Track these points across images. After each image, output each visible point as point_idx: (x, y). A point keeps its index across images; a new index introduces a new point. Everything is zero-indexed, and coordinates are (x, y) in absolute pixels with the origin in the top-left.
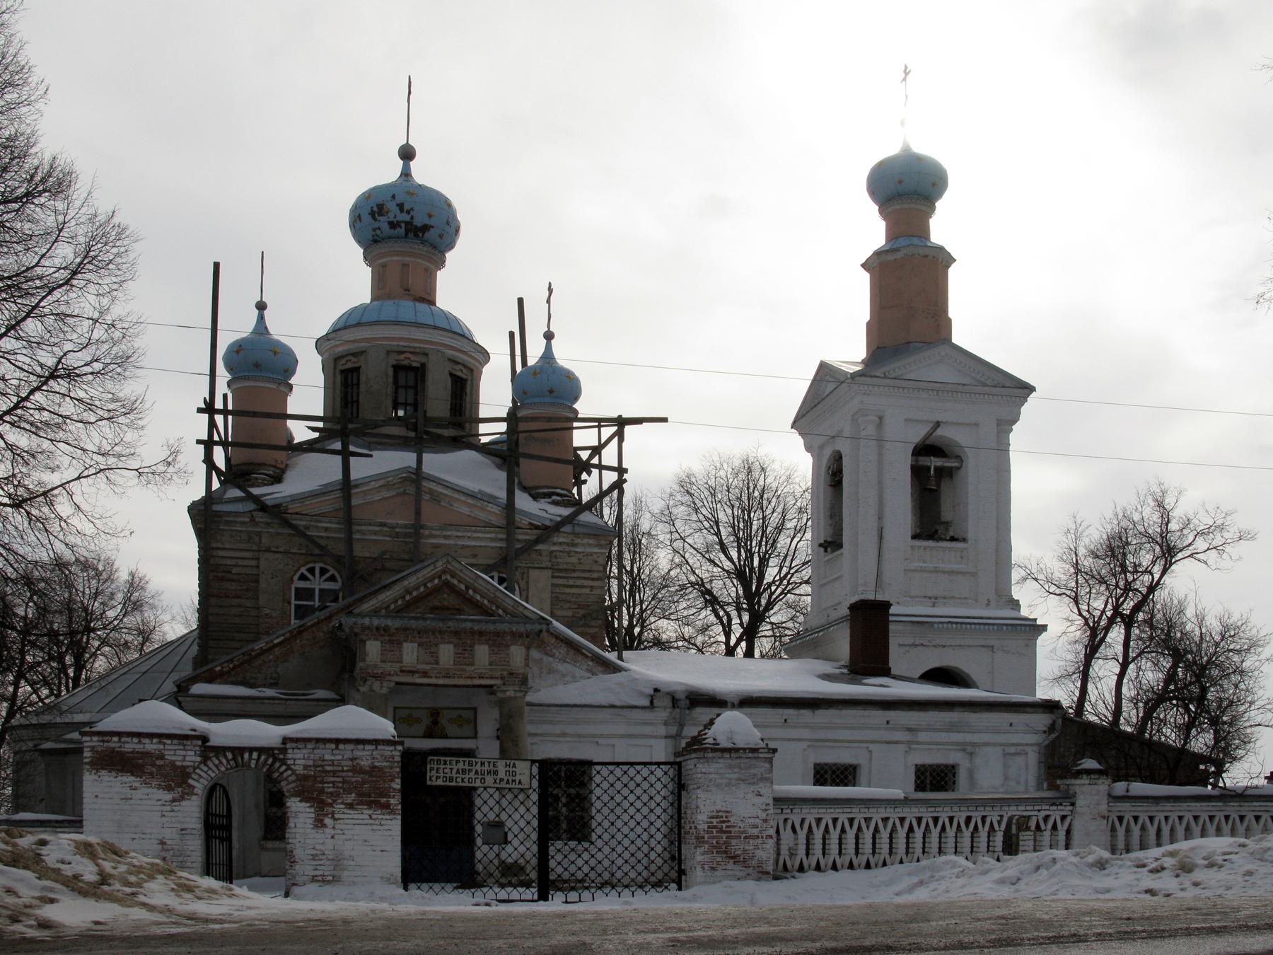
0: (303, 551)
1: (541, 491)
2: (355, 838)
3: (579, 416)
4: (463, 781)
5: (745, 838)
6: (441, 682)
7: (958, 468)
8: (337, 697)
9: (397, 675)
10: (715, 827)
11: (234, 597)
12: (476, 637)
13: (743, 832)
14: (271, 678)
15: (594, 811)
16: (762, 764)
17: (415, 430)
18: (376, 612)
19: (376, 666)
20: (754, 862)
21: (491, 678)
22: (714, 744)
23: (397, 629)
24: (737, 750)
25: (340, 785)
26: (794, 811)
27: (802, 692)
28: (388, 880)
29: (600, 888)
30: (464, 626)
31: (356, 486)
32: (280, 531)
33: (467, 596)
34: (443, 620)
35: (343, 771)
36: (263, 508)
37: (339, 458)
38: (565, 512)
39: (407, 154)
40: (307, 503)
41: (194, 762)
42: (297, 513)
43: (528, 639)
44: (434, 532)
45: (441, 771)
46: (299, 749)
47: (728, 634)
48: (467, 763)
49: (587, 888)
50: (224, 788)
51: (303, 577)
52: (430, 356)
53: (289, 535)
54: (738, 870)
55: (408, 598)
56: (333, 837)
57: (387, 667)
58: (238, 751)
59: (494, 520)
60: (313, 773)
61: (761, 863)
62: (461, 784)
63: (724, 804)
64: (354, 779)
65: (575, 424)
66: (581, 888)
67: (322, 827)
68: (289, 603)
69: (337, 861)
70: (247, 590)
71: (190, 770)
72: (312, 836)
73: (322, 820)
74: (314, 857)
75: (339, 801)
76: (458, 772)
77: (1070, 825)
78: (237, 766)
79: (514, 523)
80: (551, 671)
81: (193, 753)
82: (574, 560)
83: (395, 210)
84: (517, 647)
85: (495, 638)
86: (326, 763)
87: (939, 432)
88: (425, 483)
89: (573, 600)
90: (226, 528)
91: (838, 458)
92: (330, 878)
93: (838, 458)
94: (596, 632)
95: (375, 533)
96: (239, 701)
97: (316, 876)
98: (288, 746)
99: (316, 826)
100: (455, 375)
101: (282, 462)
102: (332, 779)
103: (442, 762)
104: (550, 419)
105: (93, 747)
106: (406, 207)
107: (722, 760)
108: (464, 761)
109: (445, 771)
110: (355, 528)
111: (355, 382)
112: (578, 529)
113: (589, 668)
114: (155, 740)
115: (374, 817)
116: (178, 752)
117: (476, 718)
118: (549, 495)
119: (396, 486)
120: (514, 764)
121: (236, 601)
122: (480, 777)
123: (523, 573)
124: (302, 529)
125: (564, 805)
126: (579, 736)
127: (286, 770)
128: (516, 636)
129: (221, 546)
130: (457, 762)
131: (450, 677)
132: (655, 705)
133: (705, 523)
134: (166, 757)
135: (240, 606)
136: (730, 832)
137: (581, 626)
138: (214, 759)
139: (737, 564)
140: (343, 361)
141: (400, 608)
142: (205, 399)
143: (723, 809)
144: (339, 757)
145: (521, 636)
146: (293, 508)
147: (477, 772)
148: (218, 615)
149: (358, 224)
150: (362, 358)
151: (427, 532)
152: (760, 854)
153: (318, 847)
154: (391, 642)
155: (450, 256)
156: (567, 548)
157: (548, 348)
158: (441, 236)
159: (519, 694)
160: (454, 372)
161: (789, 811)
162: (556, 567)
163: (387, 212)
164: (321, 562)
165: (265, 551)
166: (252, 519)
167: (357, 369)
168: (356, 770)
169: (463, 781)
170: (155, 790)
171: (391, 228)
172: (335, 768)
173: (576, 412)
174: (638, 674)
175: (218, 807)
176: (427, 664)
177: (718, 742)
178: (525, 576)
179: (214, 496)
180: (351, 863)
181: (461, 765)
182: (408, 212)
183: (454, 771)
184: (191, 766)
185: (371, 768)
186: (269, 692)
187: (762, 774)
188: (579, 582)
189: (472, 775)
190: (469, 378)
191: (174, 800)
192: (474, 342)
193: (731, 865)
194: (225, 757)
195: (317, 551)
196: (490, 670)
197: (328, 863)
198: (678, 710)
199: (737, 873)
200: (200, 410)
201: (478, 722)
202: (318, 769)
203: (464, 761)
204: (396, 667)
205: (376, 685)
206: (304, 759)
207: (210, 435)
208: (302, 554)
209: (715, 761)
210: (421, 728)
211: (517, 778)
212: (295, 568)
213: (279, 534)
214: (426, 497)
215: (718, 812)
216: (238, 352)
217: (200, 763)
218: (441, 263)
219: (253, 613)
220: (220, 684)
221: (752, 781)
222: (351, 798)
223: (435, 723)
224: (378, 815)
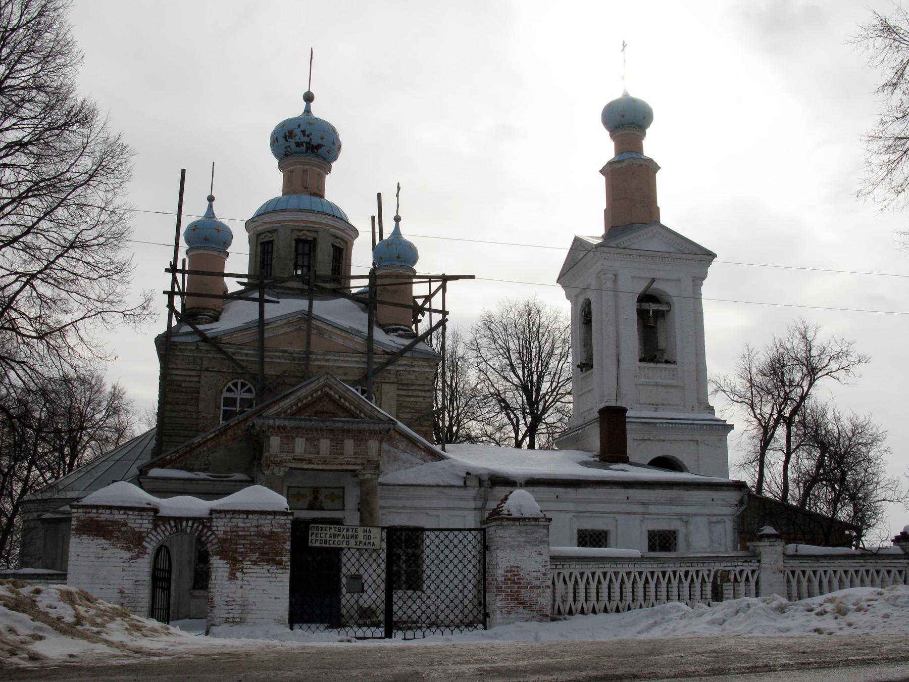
0: (231, 370)
2: (257, 588)
3: (417, 274)
4: (334, 543)
5: (531, 587)
6: (320, 467)
7: (668, 311)
8: (249, 479)
10: (509, 579)
12: (346, 434)
13: (530, 583)
15: (425, 567)
16: (542, 530)
17: (308, 284)
18: (277, 415)
19: (276, 455)
20: (537, 607)
21: (355, 464)
22: (508, 515)
23: (292, 428)
24: (524, 519)
25: (248, 546)
28: (280, 621)
29: (428, 628)
31: (268, 324)
32: (215, 356)
34: (323, 421)
35: (250, 535)
36: (205, 339)
37: (257, 304)
38: (407, 342)
39: (309, 98)
41: (148, 529)
42: (227, 343)
44: (319, 357)
47: (516, 431)
49: (419, 628)
51: (229, 390)
53: (222, 359)
54: (526, 613)
55: (300, 405)
56: (241, 587)
57: (284, 456)
58: (179, 520)
60: (229, 537)
61: (542, 608)
62: (332, 546)
64: (258, 542)
65: (414, 280)
66: (415, 628)
68: (219, 409)
69: (244, 607)
71: (144, 535)
72: (226, 586)
73: (234, 574)
76: (330, 536)
77: (758, 577)
80: (396, 459)
81: (147, 522)
82: (412, 377)
86: (239, 529)
87: (655, 285)
88: (314, 322)
91: (588, 304)
92: (238, 620)
93: (588, 304)
95: (279, 357)
96: (181, 481)
97: (228, 618)
98: (214, 516)
99: (230, 579)
104: (397, 277)
105: (78, 517)
106: (307, 133)
107: (513, 527)
110: (266, 354)
111: (270, 250)
112: (415, 355)
114: (122, 512)
115: (271, 571)
117: (344, 494)
118: (396, 330)
121: (183, 407)
122: (346, 540)
124: (230, 354)
125: (404, 562)
126: (416, 508)
127: (211, 535)
128: (373, 433)
129: (175, 367)
130: (330, 528)
131: (326, 464)
134: (129, 525)
135: (186, 411)
136: (520, 583)
138: (162, 526)
140: (263, 237)
143: (515, 565)
144: (249, 525)
145: (376, 432)
146: (225, 339)
147: (343, 536)
148: (170, 417)
150: (275, 234)
151: (314, 357)
153: (231, 595)
154: (287, 437)
156: (408, 369)
158: (329, 152)
161: (561, 567)
163: (295, 136)
166: (197, 348)
167: (271, 242)
168: (260, 535)
169: (334, 543)
172: (245, 533)
173: (415, 272)
176: (312, 454)
179: (172, 330)
180: (253, 607)
181: (333, 531)
182: (308, 136)
183: (328, 536)
186: (203, 475)
187: (541, 538)
188: (415, 393)
189: (340, 538)
191: (132, 558)
193: (521, 610)
194: (170, 525)
195: (240, 371)
196: (355, 458)
197: (238, 607)
198: (483, 489)
200: (167, 270)
205: (276, 470)
207: (173, 288)
210: (305, 503)
211: (371, 541)
213: (214, 358)
214: (314, 331)
215: (511, 567)
216: (194, 230)
217: (152, 529)
218: (328, 170)
220: (169, 468)
221: (535, 543)
223: (316, 498)
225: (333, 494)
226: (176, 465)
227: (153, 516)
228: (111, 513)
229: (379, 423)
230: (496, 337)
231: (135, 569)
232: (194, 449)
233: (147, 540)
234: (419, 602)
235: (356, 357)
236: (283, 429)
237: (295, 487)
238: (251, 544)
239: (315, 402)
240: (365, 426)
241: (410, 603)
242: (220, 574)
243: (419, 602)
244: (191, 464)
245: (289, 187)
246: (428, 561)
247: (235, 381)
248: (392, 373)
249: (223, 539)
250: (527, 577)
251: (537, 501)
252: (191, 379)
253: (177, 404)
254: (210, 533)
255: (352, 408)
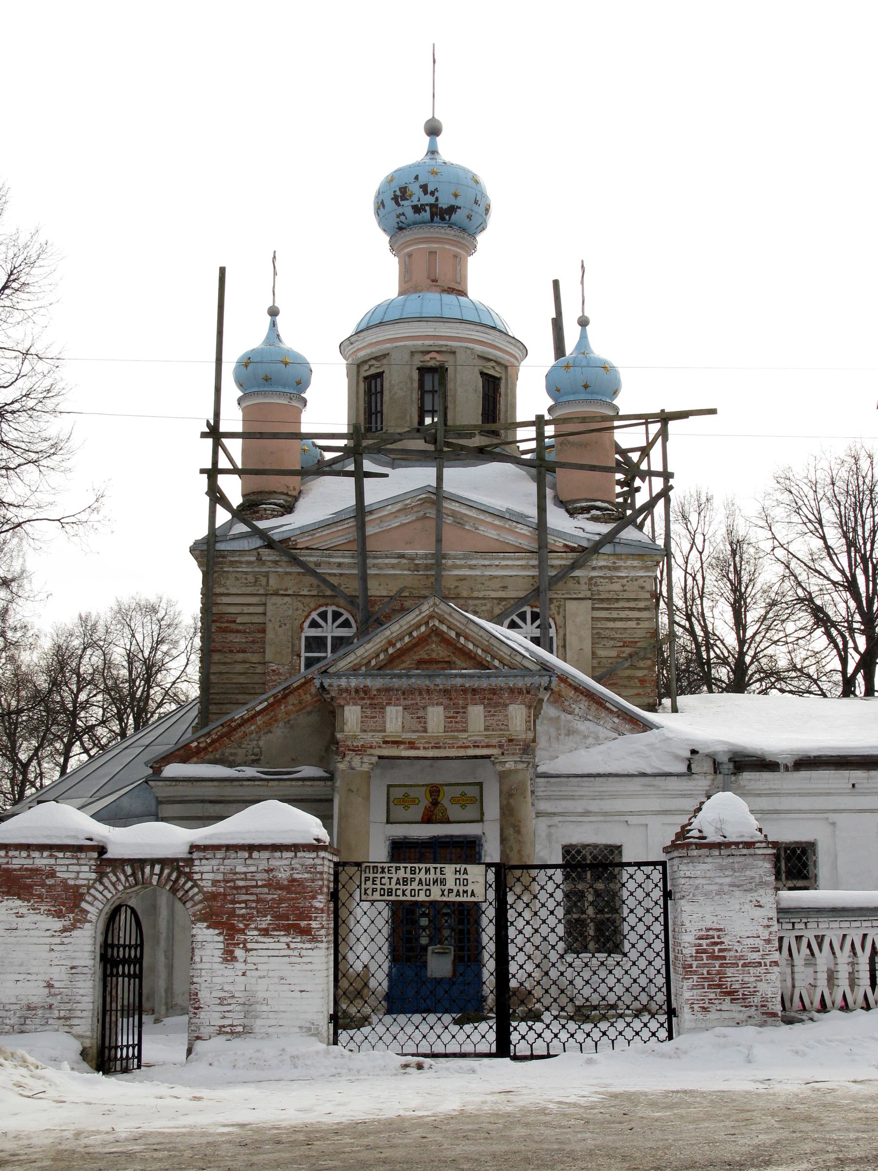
0: (314, 593)
1: (578, 505)
2: (271, 974)
3: (620, 414)
4: (404, 894)
5: (744, 965)
6: (430, 753)
8: (326, 775)
9: (380, 747)
10: (705, 951)
11: (238, 652)
12: (469, 696)
13: (741, 958)
14: (253, 754)
15: (626, 911)
16: (760, 863)
17: (435, 442)
18: (355, 670)
19: (355, 737)
20: (756, 1000)
21: (488, 746)
22: (699, 838)
23: (378, 690)
24: (728, 845)
25: (254, 905)
26: (809, 925)
27: (871, 747)
28: (309, 1029)
29: (636, 1016)
30: (454, 683)
31: (371, 512)
32: (288, 570)
33: (459, 645)
34: (429, 676)
35: (257, 886)
36: (270, 544)
37: (351, 481)
38: (605, 528)
39: (433, 130)
40: (317, 535)
41: (89, 880)
42: (307, 548)
43: (529, 696)
44: (458, 562)
45: (378, 882)
46: (207, 859)
47: (844, 661)
48: (408, 870)
49: (621, 1016)
50: (133, 911)
51: (314, 624)
52: (458, 355)
53: (299, 574)
54: (735, 1011)
56: (244, 974)
57: (369, 738)
58: (138, 864)
59: (525, 544)
60: (222, 890)
61: (765, 1000)
62: (402, 898)
63: (715, 919)
64: (270, 897)
66: (613, 1016)
67: (231, 960)
68: (299, 656)
69: (249, 1006)
70: (253, 642)
71: (83, 890)
72: (219, 973)
73: (232, 952)
74: (222, 1001)
75: (252, 926)
76: (398, 883)
78: (136, 884)
79: (546, 547)
80: (570, 732)
81: (86, 868)
82: (617, 587)
83: (418, 192)
84: (517, 707)
85: (491, 696)
86: (238, 876)
88: (446, 504)
89: (618, 636)
90: (231, 569)
92: (240, 1029)
94: (645, 676)
95: (393, 567)
96: (215, 783)
97: (224, 1026)
98: (195, 856)
99: (226, 960)
100: (487, 374)
101: (294, 489)
102: (245, 897)
103: (380, 870)
104: (584, 420)
106: (430, 188)
107: (709, 860)
108: (406, 868)
109: (383, 881)
110: (370, 562)
111: (379, 389)
112: (619, 549)
113: (615, 726)
114: (46, 854)
115: (292, 945)
116: (71, 868)
117: (481, 796)
118: (587, 510)
119: (415, 509)
120: (465, 869)
121: (239, 657)
122: (425, 887)
123: (559, 607)
124: (312, 566)
125: (592, 903)
126: (605, 814)
127: (191, 888)
128: (515, 692)
129: (226, 592)
130: (397, 869)
131: (439, 748)
132: (693, 771)
133: (809, 524)
134: (58, 874)
135: (244, 662)
136: (724, 958)
137: (627, 668)
138: (111, 875)
139: (848, 575)
140: (366, 367)
141: (382, 663)
142: (208, 422)
143: (715, 926)
144: (253, 869)
145: (520, 691)
146: (303, 542)
148: (221, 673)
149: (382, 211)
150: (385, 361)
151: (450, 562)
152: (763, 988)
153: (226, 988)
154: (373, 706)
155: (481, 238)
156: (608, 573)
157: (583, 337)
158: (469, 217)
159: (521, 766)
160: (486, 371)
161: (802, 926)
162: (597, 597)
163: (411, 196)
164: (333, 604)
165: (272, 594)
166: (259, 559)
167: (380, 375)
168: (272, 885)
169: (404, 894)
170: (44, 917)
171: (415, 212)
172: (249, 883)
173: (616, 409)
174: (671, 731)
175: (125, 934)
176: (414, 731)
177: (704, 834)
178: (561, 610)
179: (217, 533)
181: (401, 874)
182: (432, 193)
183: (394, 881)
184: (84, 885)
185: (289, 881)
186: (250, 772)
187: (761, 877)
188: (623, 614)
189: (415, 885)
190: (504, 377)
191: (65, 930)
192: (507, 335)
193: (727, 1005)
194: (124, 872)
195: (329, 592)
196: (487, 736)
197: (239, 1008)
198: (720, 777)
199: (736, 1015)
200: (204, 435)
201: (484, 801)
202: (228, 885)
203: (406, 868)
204: (378, 738)
205: (356, 761)
206: (213, 872)
207: (215, 462)
208: (314, 596)
209: (701, 860)
210: (417, 812)
211: (469, 888)
212: (305, 614)
213: (289, 573)
214: (449, 520)
215: (708, 930)
216: (246, 365)
217: (95, 880)
218: (471, 248)
219: (260, 669)
220: (196, 763)
221: (749, 886)
222: (265, 922)
223: (435, 803)
224: (297, 942)
225: (463, 794)
226: (207, 757)
227: (96, 859)
228: (29, 856)
229: (524, 676)
230: (800, 503)
231: (69, 947)
232: (235, 729)
233: (88, 898)
234: (618, 972)
235: (518, 559)
236: (365, 692)
237: (400, 786)
238: (258, 901)
239: (415, 645)
240: (500, 682)
241: (603, 973)
242: (209, 952)
243: (618, 972)
244: (231, 754)
245: (408, 286)
246: (631, 902)
247: (323, 609)
248: (582, 581)
249: (212, 892)
250: (737, 947)
251: (752, 812)
252: (252, 610)
253: (231, 651)
254: (190, 884)
255: (479, 652)
